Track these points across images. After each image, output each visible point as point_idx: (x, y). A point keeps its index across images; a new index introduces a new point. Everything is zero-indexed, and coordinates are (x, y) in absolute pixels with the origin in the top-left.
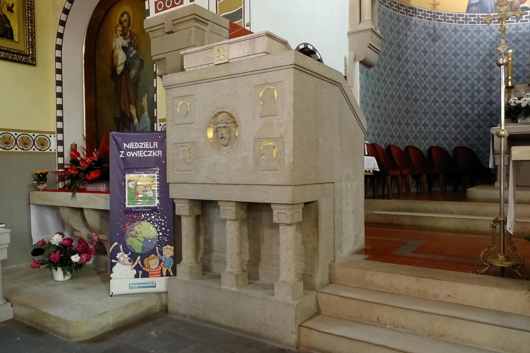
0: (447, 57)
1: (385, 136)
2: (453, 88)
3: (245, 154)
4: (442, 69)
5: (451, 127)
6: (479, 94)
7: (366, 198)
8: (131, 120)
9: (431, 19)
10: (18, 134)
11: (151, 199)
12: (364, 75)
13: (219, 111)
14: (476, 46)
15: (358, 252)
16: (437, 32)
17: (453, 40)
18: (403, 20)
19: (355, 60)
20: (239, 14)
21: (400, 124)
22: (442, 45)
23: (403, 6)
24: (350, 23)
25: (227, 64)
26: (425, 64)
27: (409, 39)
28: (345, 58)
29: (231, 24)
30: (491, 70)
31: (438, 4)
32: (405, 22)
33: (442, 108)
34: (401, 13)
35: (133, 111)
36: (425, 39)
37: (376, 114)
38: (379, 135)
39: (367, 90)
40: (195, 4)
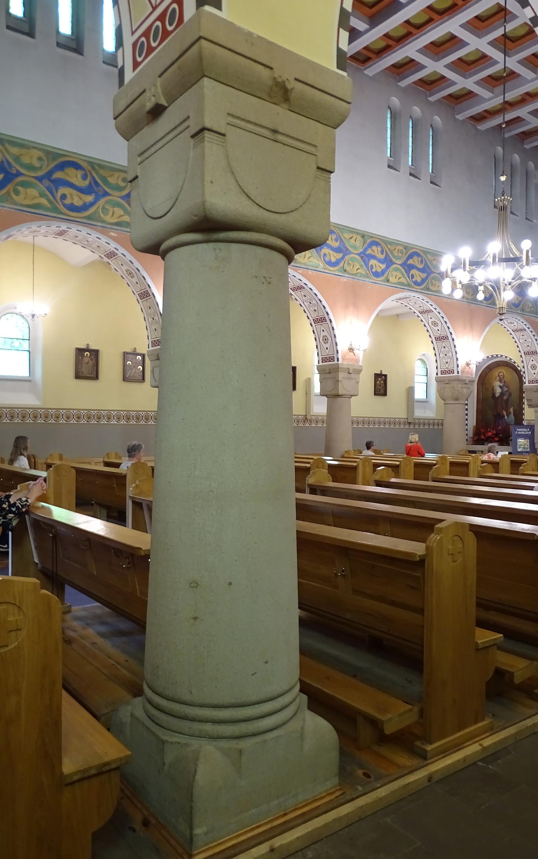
8: (504, 416)
10: (20, 410)
11: (527, 448)
25: (160, 72)
35: (505, 413)
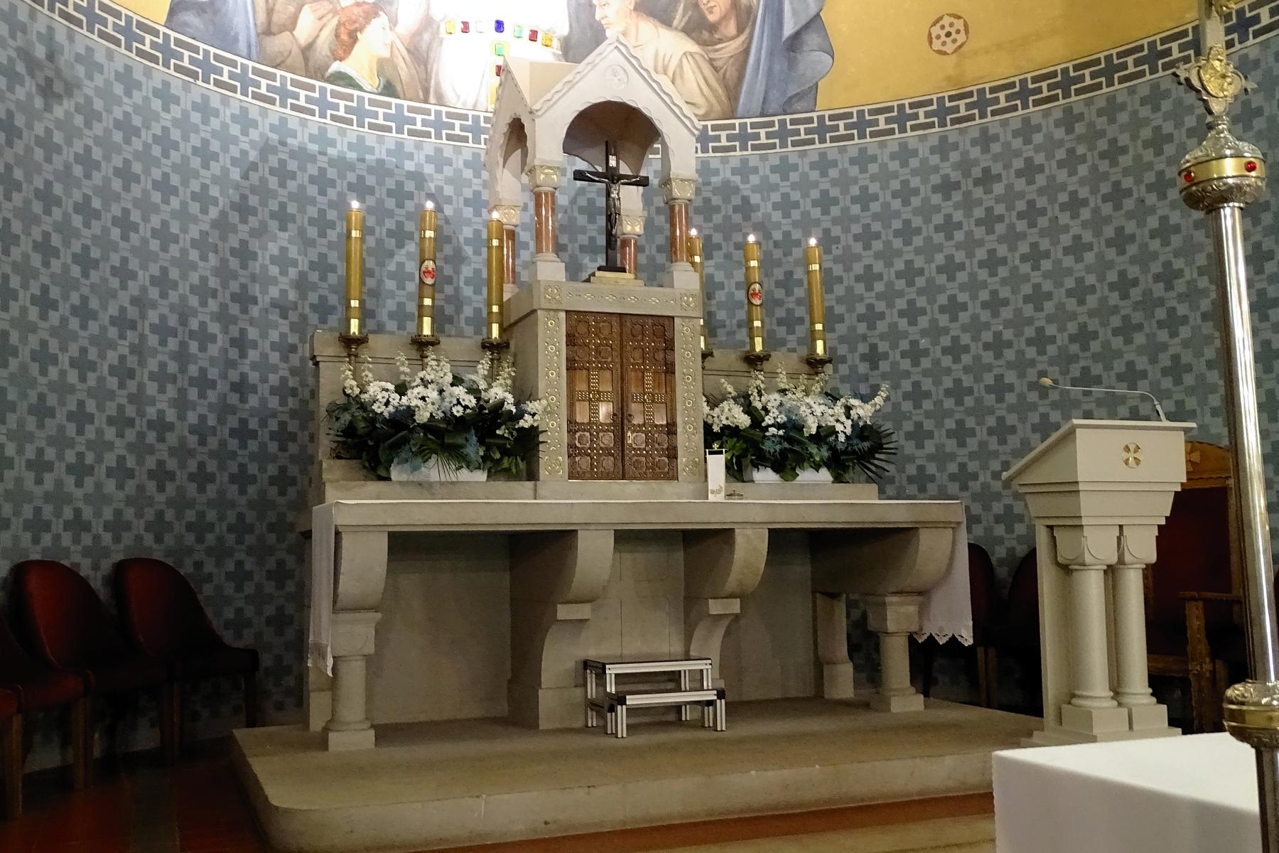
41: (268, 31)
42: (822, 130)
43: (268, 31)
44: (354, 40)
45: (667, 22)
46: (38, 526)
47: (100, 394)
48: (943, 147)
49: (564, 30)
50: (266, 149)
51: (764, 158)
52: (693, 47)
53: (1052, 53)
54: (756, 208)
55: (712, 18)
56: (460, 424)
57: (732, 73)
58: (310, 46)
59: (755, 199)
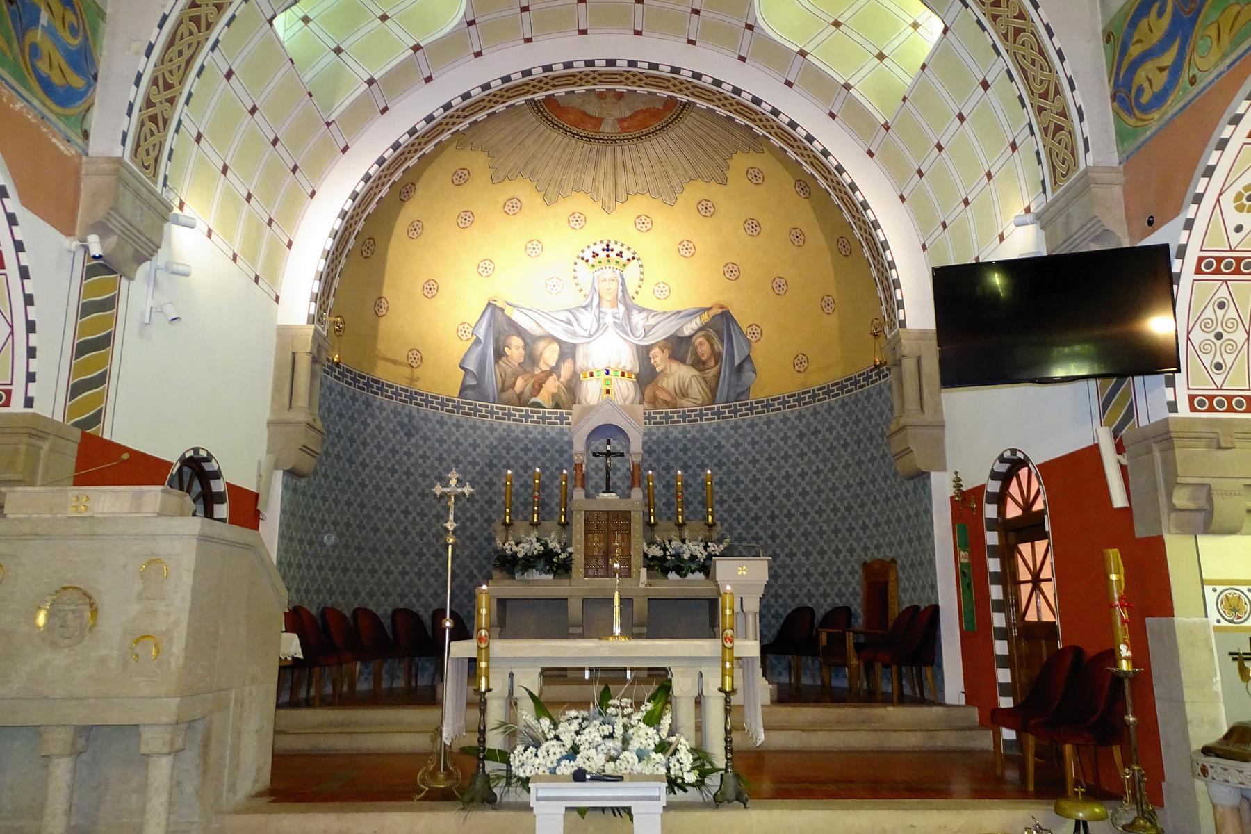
0: (428, 462)
1: (318, 591)
2: (434, 512)
3: (104, 652)
4: (420, 480)
5: (428, 575)
6: (472, 524)
7: (278, 706)
9: (405, 401)
12: (290, 492)
13: (66, 585)
14: (470, 449)
15: (260, 795)
16: (415, 422)
17: (437, 436)
18: (361, 399)
19: (276, 467)
20: (97, 418)
21: (345, 570)
22: (421, 442)
23: (363, 377)
24: (272, 406)
26: (393, 471)
27: (369, 430)
28: (260, 463)
29: (84, 434)
30: (491, 488)
31: (418, 379)
32: (364, 403)
33: (417, 544)
34: (360, 388)
36: (394, 432)
37: (304, 554)
38: (307, 591)
39: (293, 514)
40: (34, 415)
41: (503, 390)
42: (752, 409)
43: (503, 390)
44: (541, 387)
45: (683, 362)
46: (402, 596)
47: (429, 545)
48: (800, 416)
49: (637, 370)
50: (501, 439)
51: (727, 423)
52: (696, 372)
53: (837, 374)
54: (723, 447)
55: (704, 359)
56: (539, 556)
57: (713, 385)
58: (522, 392)
59: (724, 442)
